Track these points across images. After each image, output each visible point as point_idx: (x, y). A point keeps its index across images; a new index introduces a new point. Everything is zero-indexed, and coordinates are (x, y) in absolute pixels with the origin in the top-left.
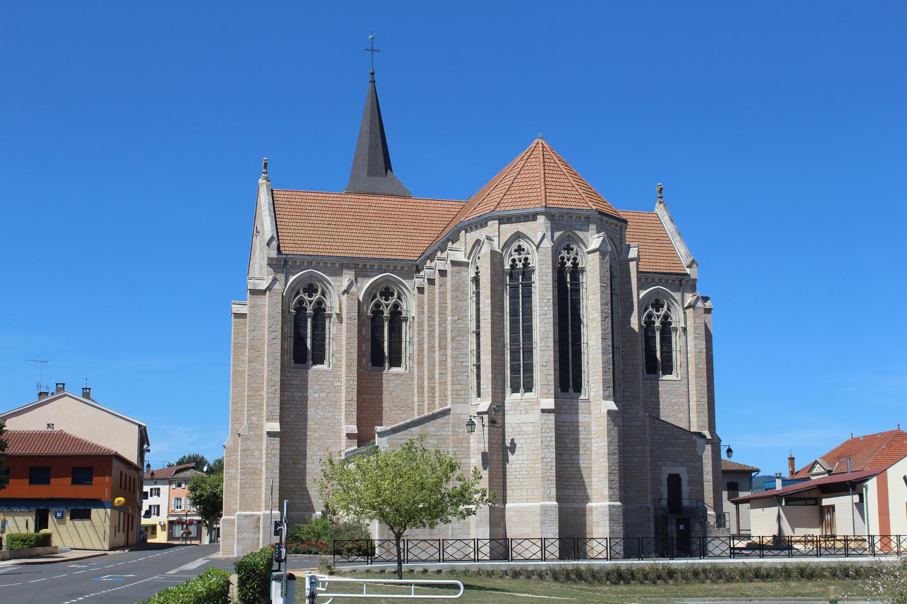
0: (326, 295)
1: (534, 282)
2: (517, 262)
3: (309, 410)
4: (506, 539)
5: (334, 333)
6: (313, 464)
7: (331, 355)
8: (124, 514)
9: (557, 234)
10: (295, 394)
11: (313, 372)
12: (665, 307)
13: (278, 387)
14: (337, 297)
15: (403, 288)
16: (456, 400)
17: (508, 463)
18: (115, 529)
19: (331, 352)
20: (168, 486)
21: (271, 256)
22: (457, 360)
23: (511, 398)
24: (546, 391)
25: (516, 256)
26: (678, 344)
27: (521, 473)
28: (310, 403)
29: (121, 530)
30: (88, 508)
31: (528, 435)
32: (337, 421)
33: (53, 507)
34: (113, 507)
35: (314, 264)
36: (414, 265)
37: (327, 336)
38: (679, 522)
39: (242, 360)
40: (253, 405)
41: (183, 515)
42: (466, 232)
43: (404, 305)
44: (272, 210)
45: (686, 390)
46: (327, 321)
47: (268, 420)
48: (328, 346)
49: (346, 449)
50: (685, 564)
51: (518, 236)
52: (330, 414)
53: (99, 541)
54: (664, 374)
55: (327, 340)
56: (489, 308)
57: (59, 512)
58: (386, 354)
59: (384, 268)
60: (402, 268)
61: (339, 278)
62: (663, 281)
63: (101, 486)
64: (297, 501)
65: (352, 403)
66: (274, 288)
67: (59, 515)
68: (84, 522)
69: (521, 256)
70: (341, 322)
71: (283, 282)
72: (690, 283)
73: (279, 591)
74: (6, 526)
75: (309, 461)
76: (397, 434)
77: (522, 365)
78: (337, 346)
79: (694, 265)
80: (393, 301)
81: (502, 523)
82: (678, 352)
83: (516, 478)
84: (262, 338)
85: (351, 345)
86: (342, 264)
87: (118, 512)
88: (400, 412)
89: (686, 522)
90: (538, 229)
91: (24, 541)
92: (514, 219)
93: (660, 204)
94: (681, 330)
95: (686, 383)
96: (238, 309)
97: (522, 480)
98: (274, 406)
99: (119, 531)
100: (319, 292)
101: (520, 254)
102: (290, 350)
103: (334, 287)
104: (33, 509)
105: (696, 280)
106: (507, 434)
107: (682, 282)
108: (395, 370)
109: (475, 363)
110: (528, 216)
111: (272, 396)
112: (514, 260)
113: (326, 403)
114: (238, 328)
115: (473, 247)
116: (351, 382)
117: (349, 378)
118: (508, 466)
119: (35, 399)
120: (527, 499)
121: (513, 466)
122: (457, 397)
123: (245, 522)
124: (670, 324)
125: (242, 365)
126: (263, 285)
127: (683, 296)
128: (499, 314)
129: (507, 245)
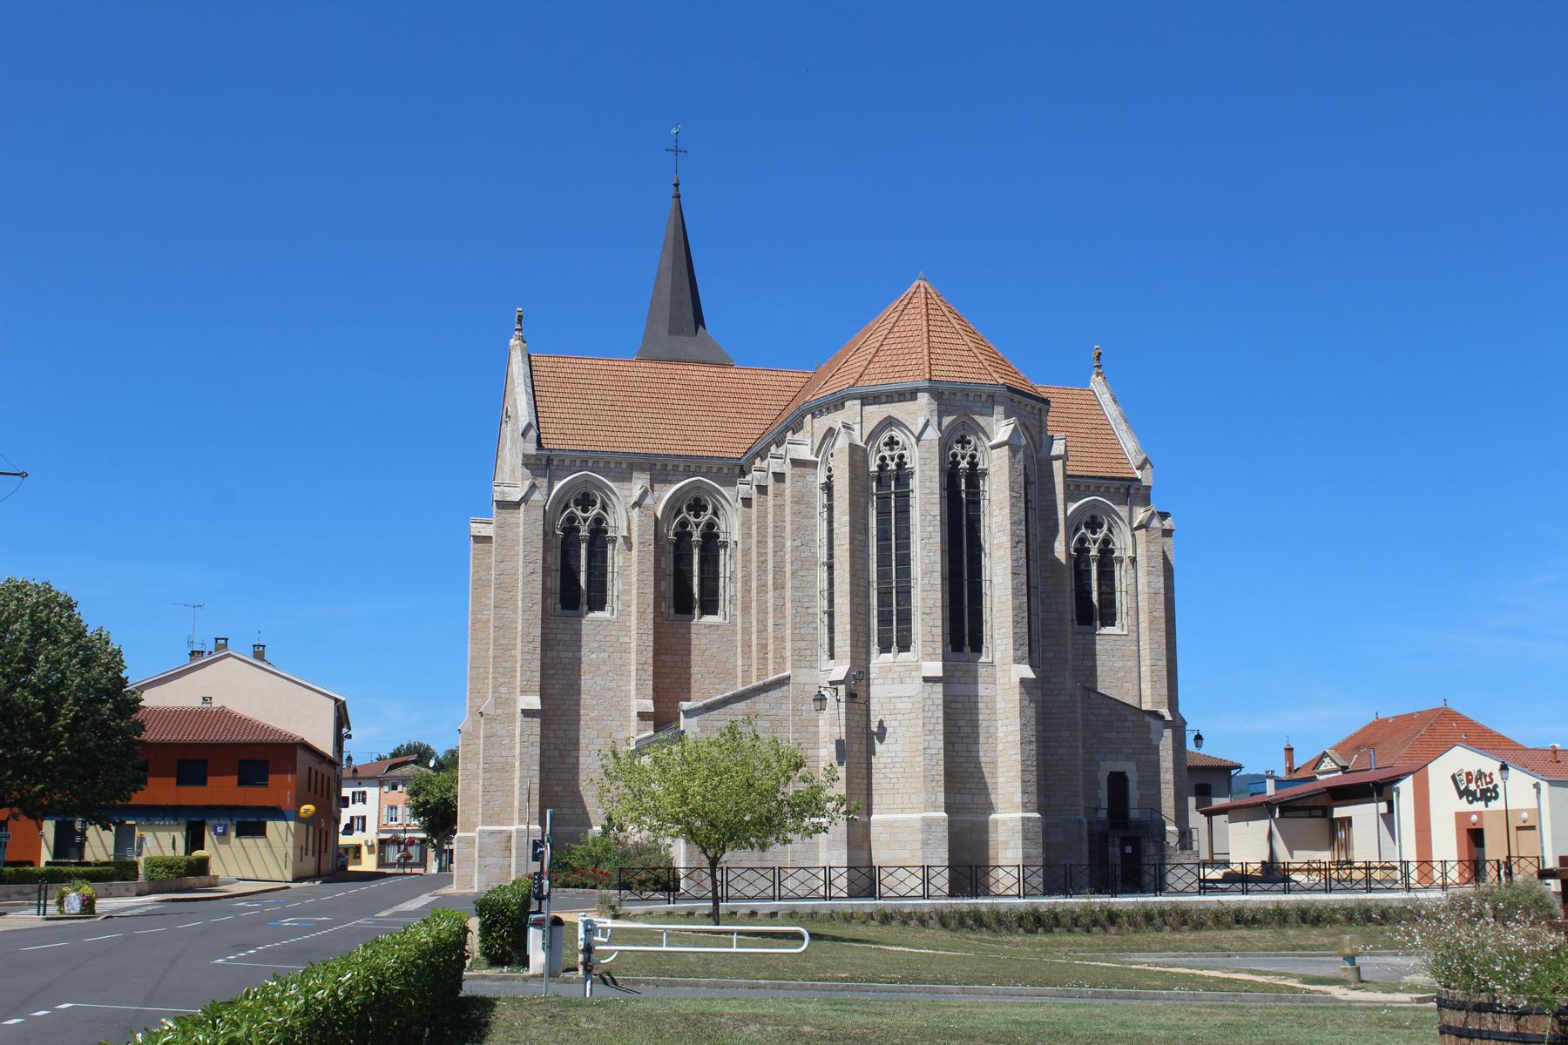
0: (608, 509)
1: (913, 491)
2: (889, 462)
3: (582, 677)
4: (872, 867)
6: (589, 756)
9: (947, 420)
12: (1105, 527)
13: (538, 644)
15: (720, 499)
16: (798, 663)
18: (301, 851)
19: (615, 593)
20: (377, 789)
21: (527, 452)
22: (799, 604)
23: (879, 661)
24: (930, 650)
25: (886, 453)
26: (1124, 581)
28: (584, 667)
29: (310, 853)
30: (262, 820)
33: (210, 818)
34: (298, 819)
35: (590, 464)
36: (736, 465)
37: (610, 569)
38: (1124, 841)
40: (501, 670)
41: (400, 831)
45: (1136, 648)
46: (610, 547)
47: (523, 692)
49: (637, 735)
51: (890, 422)
52: (613, 684)
53: (277, 868)
55: (609, 576)
56: (848, 528)
57: (220, 825)
58: (696, 596)
59: (693, 469)
60: (720, 469)
61: (626, 485)
62: (1102, 490)
63: (281, 787)
64: (565, 811)
65: (646, 667)
66: (532, 499)
67: (220, 830)
69: (894, 453)
70: (630, 549)
71: (544, 490)
73: (540, 942)
74: (144, 846)
75: (583, 752)
76: (712, 713)
77: (894, 613)
79: (1148, 466)
80: (707, 518)
81: (865, 844)
82: (1124, 593)
83: (886, 777)
84: (513, 572)
86: (632, 464)
87: (304, 826)
88: (716, 681)
89: (1136, 842)
90: (918, 413)
91: (170, 867)
92: (884, 399)
93: (1098, 376)
94: (1128, 561)
95: (1135, 639)
96: (479, 530)
97: (894, 780)
98: (532, 671)
99: (307, 854)
100: (598, 505)
101: (892, 450)
102: (555, 589)
103: (620, 498)
104: (183, 822)
105: (1148, 488)
106: (872, 713)
107: (1130, 491)
108: (708, 619)
109: (826, 609)
111: (529, 657)
112: (883, 459)
115: (824, 439)
116: (644, 637)
118: (874, 760)
119: (185, 661)
121: (881, 760)
123: (489, 841)
124: (1112, 551)
125: (485, 612)
126: (516, 495)
127: (1131, 511)
128: (861, 537)
129: (873, 436)
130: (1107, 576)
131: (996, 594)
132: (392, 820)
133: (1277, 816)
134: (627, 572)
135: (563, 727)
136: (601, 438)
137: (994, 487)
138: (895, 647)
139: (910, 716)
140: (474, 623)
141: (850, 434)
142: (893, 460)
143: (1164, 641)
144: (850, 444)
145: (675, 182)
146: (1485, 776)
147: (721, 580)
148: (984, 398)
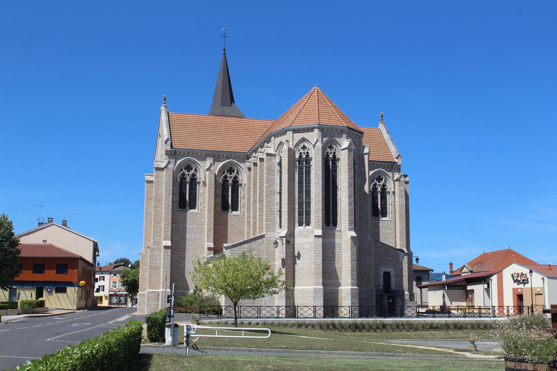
0: (197, 171)
1: (312, 166)
2: (303, 154)
3: (187, 234)
4: (294, 306)
5: (202, 192)
6: (189, 264)
7: (199, 204)
8: (85, 290)
9: (325, 139)
10: (179, 225)
11: (190, 214)
12: (384, 180)
13: (170, 222)
14: (203, 172)
17: (296, 264)
18: (80, 299)
19: (200, 203)
22: (268, 208)
23: (298, 229)
25: (302, 151)
26: (390, 200)
27: (303, 270)
28: (187, 230)
29: (83, 299)
30: (65, 287)
31: (307, 249)
32: (202, 241)
33: (45, 286)
34: (79, 286)
35: (191, 154)
36: (246, 155)
37: (198, 194)
38: (389, 298)
39: (150, 207)
41: (117, 291)
42: (275, 137)
43: (240, 177)
44: (168, 124)
45: (394, 226)
46: (198, 185)
47: (164, 239)
48: (198, 199)
49: (207, 256)
50: (392, 321)
51: (303, 140)
52: (198, 237)
54: (382, 217)
55: (197, 196)
57: (49, 288)
59: (229, 156)
61: (204, 162)
62: (383, 166)
63: (72, 274)
64: (180, 284)
65: (211, 230)
66: (168, 167)
68: (63, 294)
69: (305, 151)
70: (205, 186)
71: (173, 164)
72: (397, 167)
73: (170, 333)
74: (20, 296)
75: (186, 262)
77: (304, 211)
78: (203, 199)
79: (400, 158)
80: (234, 175)
81: (292, 297)
82: (390, 205)
85: (211, 199)
87: (81, 289)
88: (237, 236)
89: (393, 298)
90: (314, 136)
92: (301, 131)
93: (381, 124)
94: (392, 193)
96: (149, 178)
99: (82, 300)
100: (193, 170)
101: (304, 150)
103: (202, 167)
104: (35, 287)
105: (400, 166)
106: (295, 249)
107: (393, 167)
108: (235, 213)
110: (309, 129)
111: (167, 226)
112: (301, 153)
113: (196, 231)
114: (149, 188)
115: (279, 146)
117: (209, 217)
118: (296, 266)
119: (36, 226)
120: (306, 285)
121: (299, 266)
122: (269, 228)
123: (151, 295)
124: (386, 189)
125: (150, 209)
126: (163, 165)
127: (393, 174)
129: (297, 145)
130: (384, 198)
131: (342, 205)
132: (114, 287)
133: (446, 289)
134: (204, 195)
135: (179, 253)
136: (195, 144)
137: (342, 164)
138: (304, 224)
139: (310, 250)
140: (146, 213)
141: (288, 144)
142: (304, 154)
143: (405, 223)
144: (288, 148)
145: (224, 48)
146: (524, 275)
147: (239, 198)
148: (339, 131)
